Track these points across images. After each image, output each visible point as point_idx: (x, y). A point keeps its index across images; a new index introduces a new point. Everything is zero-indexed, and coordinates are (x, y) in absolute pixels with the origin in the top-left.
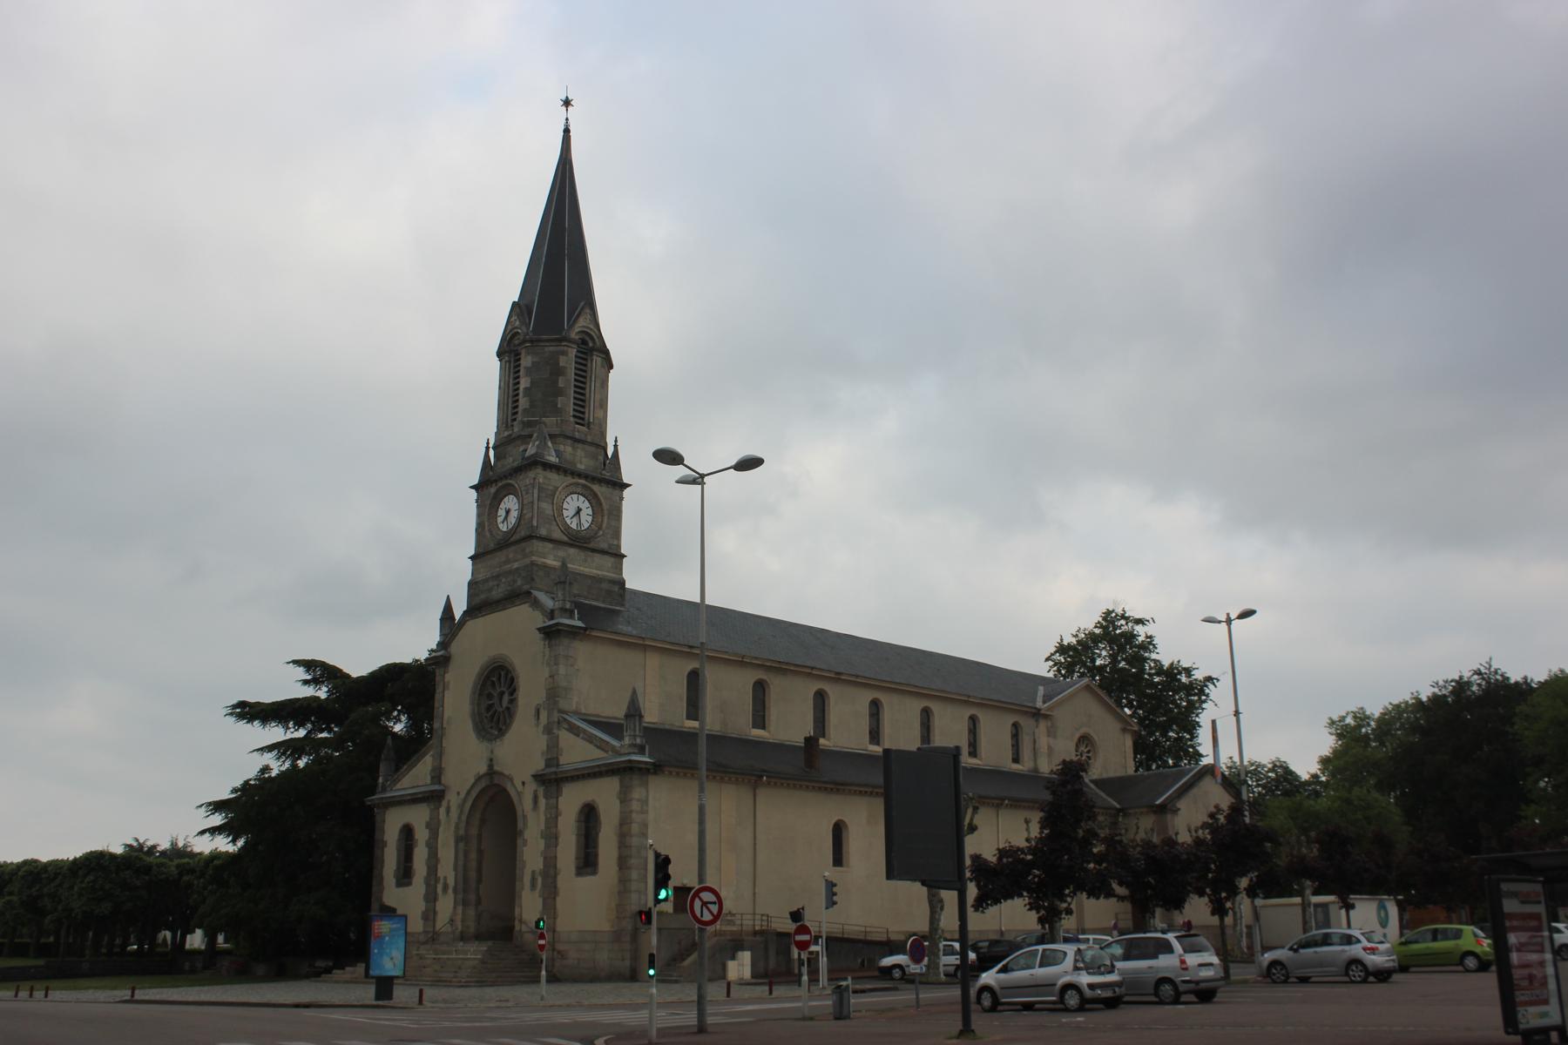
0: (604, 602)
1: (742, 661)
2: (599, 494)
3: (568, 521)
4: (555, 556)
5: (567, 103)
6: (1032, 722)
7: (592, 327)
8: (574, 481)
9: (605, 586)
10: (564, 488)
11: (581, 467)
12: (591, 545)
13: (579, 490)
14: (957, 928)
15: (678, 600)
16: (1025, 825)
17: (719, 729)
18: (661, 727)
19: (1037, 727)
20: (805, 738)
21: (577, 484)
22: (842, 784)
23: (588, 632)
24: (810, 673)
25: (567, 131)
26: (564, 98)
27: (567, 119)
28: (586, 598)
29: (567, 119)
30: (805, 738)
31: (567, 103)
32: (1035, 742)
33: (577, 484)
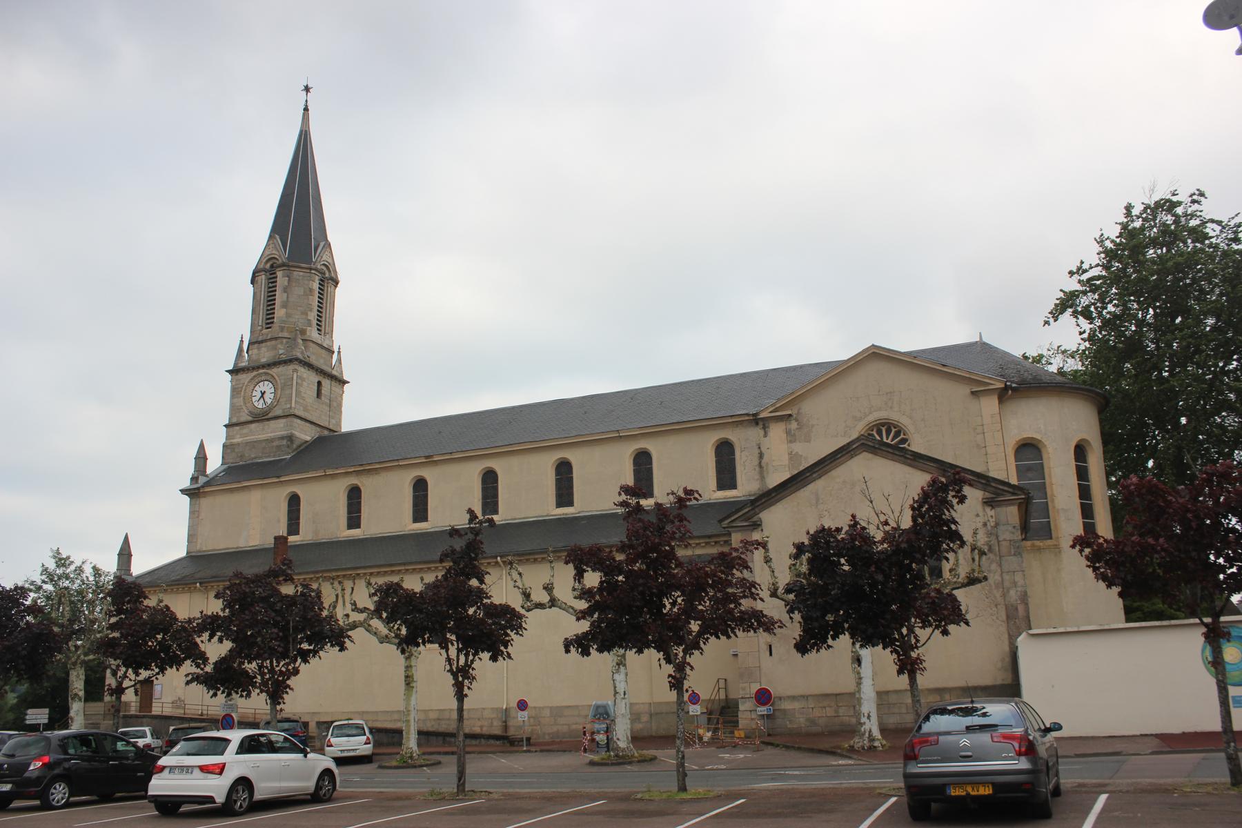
0: (274, 456)
1: (325, 475)
2: (274, 374)
3: (256, 404)
4: (241, 435)
5: (307, 89)
6: (755, 433)
7: (274, 252)
8: (256, 373)
9: (276, 443)
10: (249, 382)
11: (264, 360)
12: (270, 415)
13: (263, 378)
14: (456, 707)
15: (401, 425)
16: (1008, 539)
17: (310, 538)
18: (262, 547)
19: (765, 435)
20: (276, 538)
21: (260, 375)
22: (530, 554)
23: (201, 491)
24: (1040, 386)
25: (306, 109)
26: (305, 85)
27: (306, 101)
28: (261, 458)
29: (306, 101)
30: (276, 538)
31: (307, 89)
32: (761, 456)
33: (260, 375)
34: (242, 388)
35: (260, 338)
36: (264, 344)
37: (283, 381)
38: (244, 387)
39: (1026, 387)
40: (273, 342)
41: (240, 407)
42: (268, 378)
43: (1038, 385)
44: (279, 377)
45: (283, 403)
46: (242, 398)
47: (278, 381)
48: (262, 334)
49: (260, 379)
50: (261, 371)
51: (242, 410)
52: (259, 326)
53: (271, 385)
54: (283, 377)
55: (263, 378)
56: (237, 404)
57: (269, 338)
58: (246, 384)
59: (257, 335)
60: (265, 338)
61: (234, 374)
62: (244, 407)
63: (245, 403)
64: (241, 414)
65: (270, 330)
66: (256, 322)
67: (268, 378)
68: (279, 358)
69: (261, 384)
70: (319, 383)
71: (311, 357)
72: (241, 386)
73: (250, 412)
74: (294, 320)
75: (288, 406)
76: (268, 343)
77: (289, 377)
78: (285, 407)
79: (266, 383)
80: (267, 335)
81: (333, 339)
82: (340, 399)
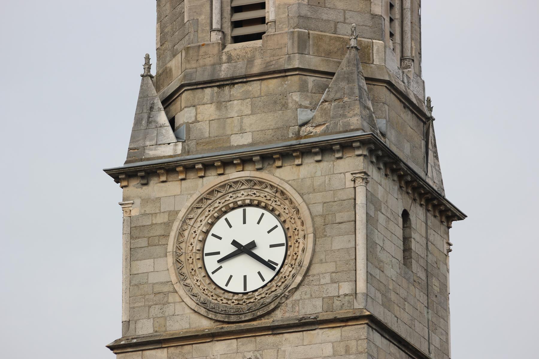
10: (193, 209)
12: (279, 317)
13: (242, 196)
34: (168, 225)
35: (225, 71)
36: (238, 90)
37: (318, 209)
38: (176, 225)
39: (419, 12)
40: (273, 84)
41: (166, 289)
42: (262, 196)
43: (287, 74)
44: (301, 195)
45: (327, 279)
46: (170, 260)
47: (303, 209)
48: (230, 59)
49: (229, 199)
50: (233, 174)
51: (171, 298)
52: (212, 30)
53: (270, 220)
54: (319, 197)
55: (242, 196)
56: (153, 278)
57: (256, 70)
58: (181, 215)
59: (209, 61)
60: (241, 69)
61: (134, 182)
62: (179, 288)
63: (182, 276)
64: (169, 310)
65: (258, 43)
66: (203, 18)
67: (262, 196)
68: (298, 136)
69: (235, 216)
70: (405, 215)
71: (388, 134)
72: (162, 219)
73: (204, 304)
74: (332, 16)
75: (346, 288)
76: (255, 87)
77: (342, 195)
78: (332, 290)
79: (253, 213)
80: (250, 62)
81: (424, 77)
82: (442, 266)
